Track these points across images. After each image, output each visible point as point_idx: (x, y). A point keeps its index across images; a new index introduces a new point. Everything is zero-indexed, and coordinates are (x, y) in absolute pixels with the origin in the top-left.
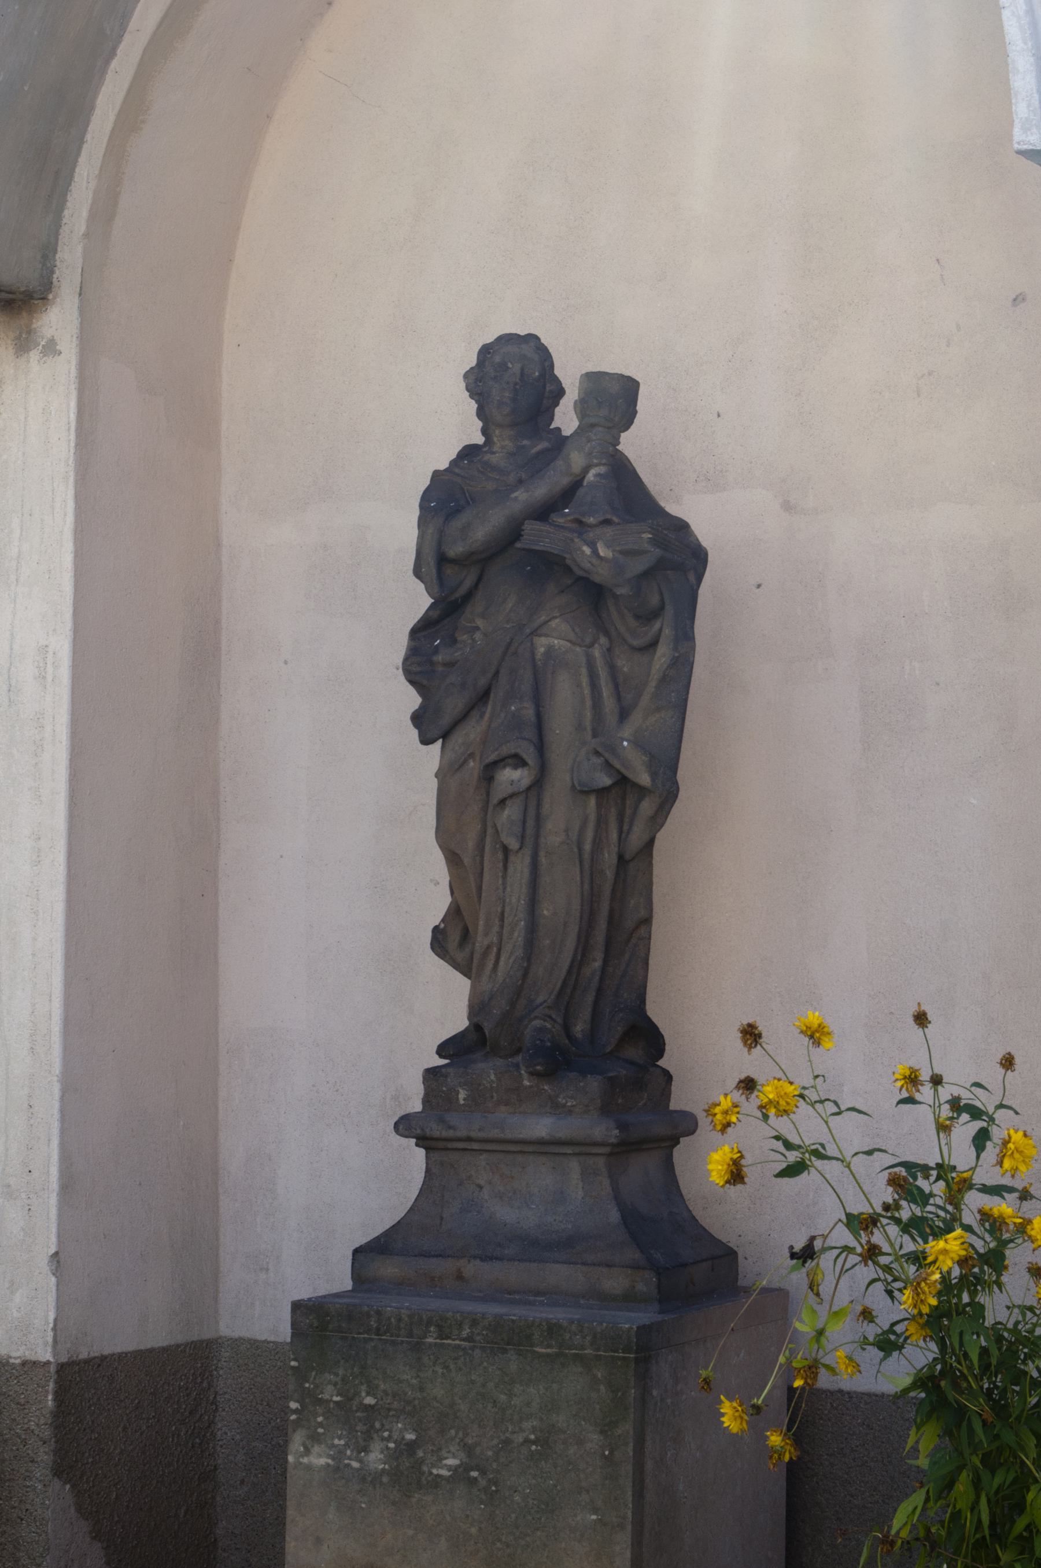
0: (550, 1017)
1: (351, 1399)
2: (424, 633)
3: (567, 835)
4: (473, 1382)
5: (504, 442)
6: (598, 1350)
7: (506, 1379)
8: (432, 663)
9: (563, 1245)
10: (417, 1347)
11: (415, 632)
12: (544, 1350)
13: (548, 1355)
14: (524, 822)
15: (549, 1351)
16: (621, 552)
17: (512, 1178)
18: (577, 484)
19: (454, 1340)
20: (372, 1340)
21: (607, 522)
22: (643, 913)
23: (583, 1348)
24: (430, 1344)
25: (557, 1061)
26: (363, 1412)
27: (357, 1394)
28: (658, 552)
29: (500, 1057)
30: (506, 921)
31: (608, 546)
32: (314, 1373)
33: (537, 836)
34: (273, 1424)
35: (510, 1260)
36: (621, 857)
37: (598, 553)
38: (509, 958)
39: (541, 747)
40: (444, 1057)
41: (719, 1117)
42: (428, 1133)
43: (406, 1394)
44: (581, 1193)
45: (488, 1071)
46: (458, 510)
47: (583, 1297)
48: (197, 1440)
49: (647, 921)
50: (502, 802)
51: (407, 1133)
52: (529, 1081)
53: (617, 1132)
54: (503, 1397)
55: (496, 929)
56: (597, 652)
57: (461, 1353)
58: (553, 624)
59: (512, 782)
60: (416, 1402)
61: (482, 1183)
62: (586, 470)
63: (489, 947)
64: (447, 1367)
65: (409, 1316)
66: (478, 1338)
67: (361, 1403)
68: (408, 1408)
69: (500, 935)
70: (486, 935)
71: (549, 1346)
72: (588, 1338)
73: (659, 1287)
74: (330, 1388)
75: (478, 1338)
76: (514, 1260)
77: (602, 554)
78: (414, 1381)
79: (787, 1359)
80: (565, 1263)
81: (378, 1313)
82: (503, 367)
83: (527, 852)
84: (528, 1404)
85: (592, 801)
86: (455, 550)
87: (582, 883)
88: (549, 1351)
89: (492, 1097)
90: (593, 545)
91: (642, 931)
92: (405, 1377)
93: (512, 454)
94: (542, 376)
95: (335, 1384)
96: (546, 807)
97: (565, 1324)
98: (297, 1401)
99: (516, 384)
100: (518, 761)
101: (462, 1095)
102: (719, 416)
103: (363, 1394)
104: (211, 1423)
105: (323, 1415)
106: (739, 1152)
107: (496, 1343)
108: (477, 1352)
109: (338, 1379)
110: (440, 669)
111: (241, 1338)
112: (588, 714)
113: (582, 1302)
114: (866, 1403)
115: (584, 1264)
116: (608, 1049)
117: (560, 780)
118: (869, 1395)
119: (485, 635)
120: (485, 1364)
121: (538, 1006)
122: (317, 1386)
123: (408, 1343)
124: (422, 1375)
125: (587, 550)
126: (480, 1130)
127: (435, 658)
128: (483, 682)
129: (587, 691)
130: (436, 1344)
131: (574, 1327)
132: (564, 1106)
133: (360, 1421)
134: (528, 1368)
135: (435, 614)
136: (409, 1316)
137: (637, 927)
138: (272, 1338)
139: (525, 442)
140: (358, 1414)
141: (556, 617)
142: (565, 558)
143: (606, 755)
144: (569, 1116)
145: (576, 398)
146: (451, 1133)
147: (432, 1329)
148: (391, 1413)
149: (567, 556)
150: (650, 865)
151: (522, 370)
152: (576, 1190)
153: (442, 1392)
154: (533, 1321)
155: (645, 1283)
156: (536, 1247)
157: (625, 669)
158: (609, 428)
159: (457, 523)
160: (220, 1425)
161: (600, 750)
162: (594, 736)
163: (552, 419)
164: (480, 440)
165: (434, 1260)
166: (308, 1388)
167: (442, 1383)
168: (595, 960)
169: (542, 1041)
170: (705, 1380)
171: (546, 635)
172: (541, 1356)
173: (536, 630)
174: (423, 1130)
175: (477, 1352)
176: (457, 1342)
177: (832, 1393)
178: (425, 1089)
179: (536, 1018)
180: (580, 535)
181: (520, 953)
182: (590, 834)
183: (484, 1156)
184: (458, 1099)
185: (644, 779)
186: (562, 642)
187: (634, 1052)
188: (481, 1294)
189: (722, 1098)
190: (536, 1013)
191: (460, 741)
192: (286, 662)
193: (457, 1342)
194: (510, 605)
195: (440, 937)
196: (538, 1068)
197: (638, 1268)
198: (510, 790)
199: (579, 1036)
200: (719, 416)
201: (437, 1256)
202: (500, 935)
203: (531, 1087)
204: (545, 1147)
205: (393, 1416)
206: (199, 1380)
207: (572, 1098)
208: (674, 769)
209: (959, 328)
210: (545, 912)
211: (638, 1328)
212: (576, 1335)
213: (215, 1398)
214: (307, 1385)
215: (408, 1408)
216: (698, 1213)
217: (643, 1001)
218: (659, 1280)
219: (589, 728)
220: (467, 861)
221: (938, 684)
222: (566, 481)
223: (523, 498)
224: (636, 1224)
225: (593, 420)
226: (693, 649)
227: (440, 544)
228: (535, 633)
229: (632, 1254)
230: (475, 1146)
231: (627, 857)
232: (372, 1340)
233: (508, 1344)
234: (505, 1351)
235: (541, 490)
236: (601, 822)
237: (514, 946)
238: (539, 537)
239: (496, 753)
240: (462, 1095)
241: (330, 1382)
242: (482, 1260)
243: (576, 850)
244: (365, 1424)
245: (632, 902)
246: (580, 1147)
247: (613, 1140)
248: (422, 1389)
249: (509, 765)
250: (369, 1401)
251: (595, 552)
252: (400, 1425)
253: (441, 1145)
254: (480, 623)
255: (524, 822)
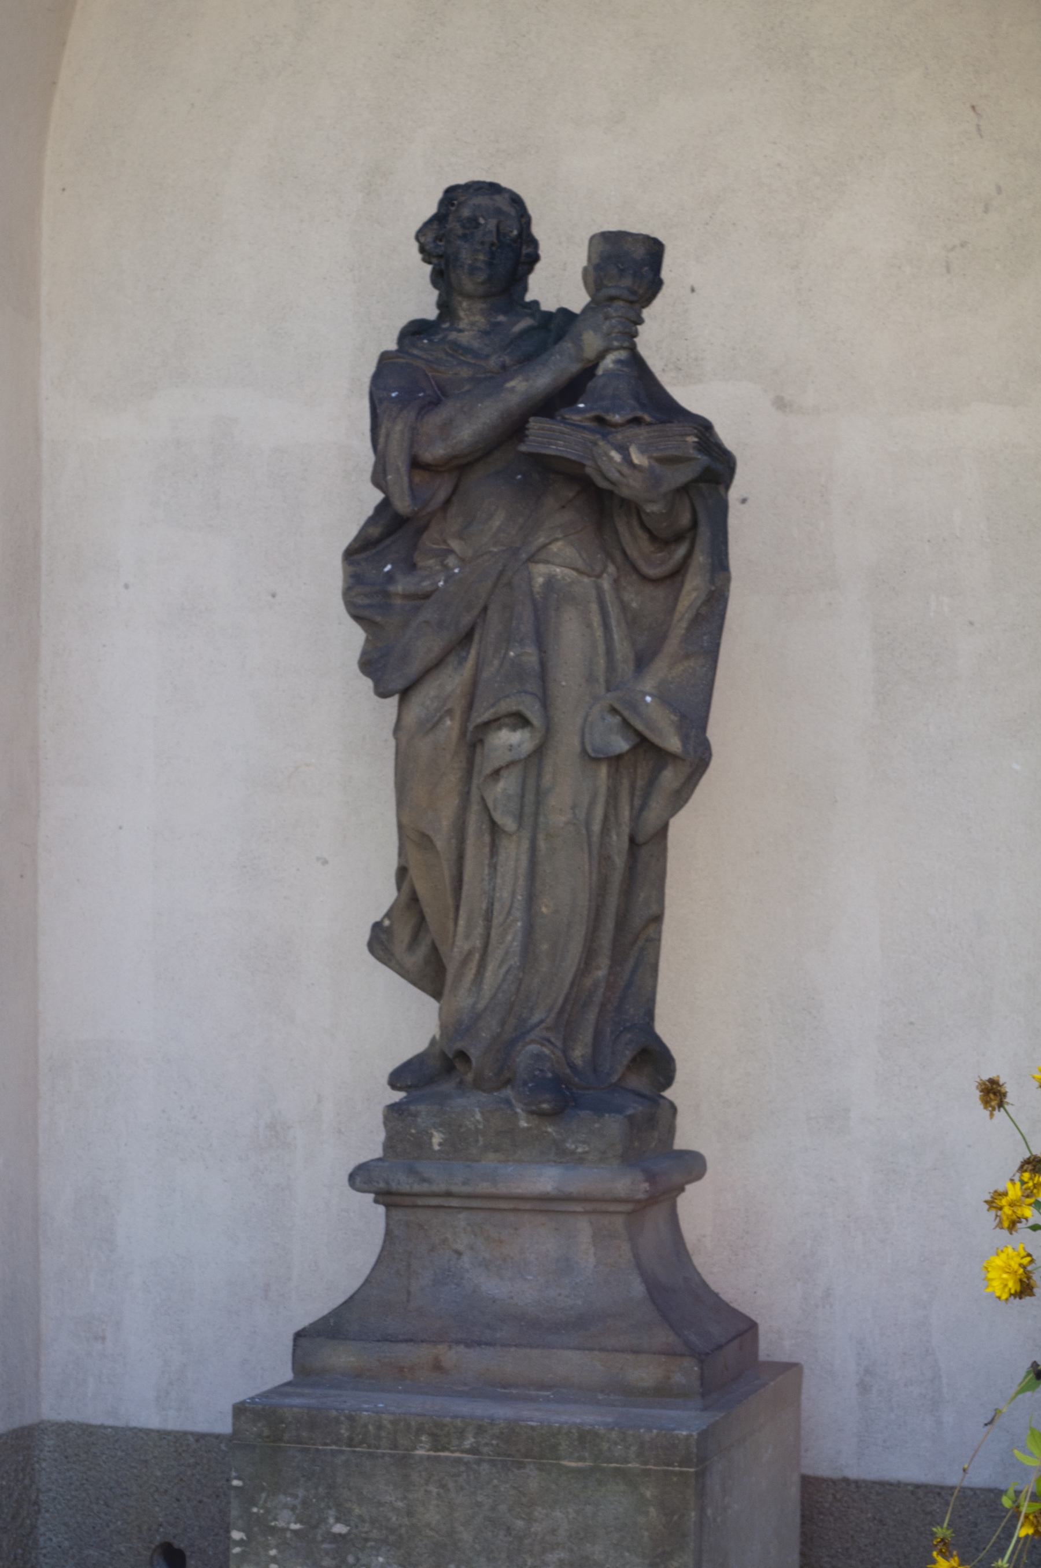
0: (549, 1041)
1: (316, 1527)
2: (363, 555)
3: (574, 813)
4: (479, 1505)
5: (471, 318)
6: (646, 1463)
7: (524, 1500)
8: (387, 594)
9: (578, 1326)
10: (404, 1461)
11: (350, 554)
12: (573, 1464)
13: (579, 1470)
14: (523, 796)
15: (580, 1464)
16: (660, 460)
17: (501, 1242)
18: (589, 371)
19: (452, 1452)
20: (342, 1452)
21: (637, 421)
22: (654, 909)
23: (626, 1461)
24: (421, 1457)
25: (563, 1096)
26: (330, 1543)
27: (323, 1520)
28: (704, 459)
29: (484, 1091)
30: (495, 922)
31: (642, 451)
32: (264, 1495)
33: (536, 814)
34: (112, 1527)
35: (503, 1345)
36: (632, 840)
37: (627, 461)
38: (500, 967)
39: (545, 702)
40: (400, 1089)
41: (1007, 1210)
42: (394, 1187)
43: (389, 1520)
44: (592, 1260)
45: (473, 1110)
46: (434, 403)
47: (602, 1392)
48: (20, 1551)
49: (657, 919)
50: (496, 773)
51: (366, 1187)
52: (528, 1122)
53: (646, 1186)
54: (520, 1523)
55: (479, 930)
56: (606, 584)
57: (463, 1468)
58: (554, 547)
59: (511, 748)
60: (403, 1530)
61: (461, 1247)
62: (601, 356)
63: (470, 953)
64: (443, 1486)
65: (392, 1422)
66: (485, 1450)
67: (329, 1533)
68: (392, 1538)
69: (487, 937)
70: (467, 936)
71: (581, 1459)
72: (634, 1449)
73: (702, 1378)
74: (286, 1514)
75: (485, 1450)
76: (510, 1346)
77: (636, 461)
78: (400, 1504)
79: (1014, 1502)
80: (579, 1349)
81: (351, 1418)
82: (473, 222)
83: (526, 834)
84: (553, 1531)
85: (603, 770)
86: (435, 452)
87: (591, 873)
88: (580, 1464)
89: (477, 1141)
90: (623, 450)
91: (651, 931)
92: (388, 1498)
93: (485, 333)
94: (520, 235)
95: (293, 1509)
96: (547, 780)
97: (602, 1430)
98: (240, 1530)
99: (493, 244)
100: (520, 720)
101: (437, 1139)
102: (693, 290)
103: (331, 1520)
104: (34, 1527)
105: (277, 1547)
106: (1029, 1255)
107: (509, 1456)
108: (485, 1466)
109: (297, 1502)
110: (398, 602)
111: (69, 1423)
112: (602, 662)
113: (600, 1397)
114: (878, 1494)
115: (602, 1350)
116: (615, 1079)
117: (567, 744)
118: (882, 1484)
119: (462, 560)
120: (495, 1482)
121: (533, 1028)
122: (268, 1511)
123: (392, 1456)
124: (410, 1496)
125: (616, 456)
126: (464, 1184)
127: (392, 588)
128: (466, 620)
129: (599, 633)
130: (429, 1457)
131: (614, 1435)
132: (573, 1153)
133: (327, 1554)
134: (554, 1487)
135: (375, 532)
136: (392, 1422)
137: (645, 927)
138: (110, 1422)
139: (501, 318)
140: (325, 1546)
141: (557, 540)
142: (583, 466)
143: (626, 714)
144: (576, 1167)
145: (585, 263)
146: (425, 1188)
147: (423, 1438)
148: (370, 1544)
149: (588, 463)
150: (664, 850)
151: (498, 227)
152: (586, 1255)
153: (438, 1517)
154: (560, 1428)
155: (684, 1373)
156: (537, 1329)
157: (634, 605)
158: (632, 302)
159: (435, 419)
160: (42, 1529)
161: (617, 706)
162: (608, 690)
163: (525, 289)
164: (431, 313)
165: (403, 1346)
166: (256, 1514)
167: (438, 1506)
168: (598, 968)
169: (542, 1071)
170: (942, 1540)
171: (547, 562)
172: (570, 1471)
173: (533, 555)
174: (387, 1183)
175: (485, 1466)
176: (457, 1455)
177: (834, 1482)
178: (387, 1132)
179: (533, 1041)
180: (604, 436)
181: (515, 961)
182: (599, 812)
183: (463, 1216)
184: (431, 1144)
185: (673, 743)
186: (567, 571)
187: (638, 1082)
188: (466, 1389)
189: (1009, 1185)
190: (532, 1036)
191: (432, 693)
192: (126, 586)
193: (457, 1455)
194: (496, 523)
195: (384, 937)
196: (545, 1106)
197: (675, 1354)
198: (508, 757)
199: (579, 1062)
200: (693, 290)
201: (406, 1341)
202: (487, 937)
203: (529, 1129)
204: (547, 1204)
205: (372, 1547)
206: (21, 1476)
207: (584, 1142)
208: (704, 728)
209: (999, 190)
210: (544, 910)
211: (699, 1434)
212: (616, 1444)
213: (37, 1497)
214: (255, 1510)
215: (392, 1538)
216: (710, 1280)
217: (650, 1014)
218: (702, 1369)
219: (602, 680)
220: (440, 844)
221: (971, 623)
222: (575, 368)
223: (521, 388)
224: (659, 1294)
225: (613, 292)
226: (728, 580)
227: (412, 443)
228: (532, 559)
229: (663, 1337)
230: (454, 1202)
231: (640, 839)
232: (342, 1452)
233: (526, 1457)
234: (521, 1465)
235: (541, 379)
236: (613, 796)
237: (507, 953)
238: (546, 437)
239: (492, 710)
240: (437, 1139)
241: (285, 1506)
242: (467, 1345)
243: (584, 831)
244: (334, 1558)
245: (642, 895)
246: (592, 1204)
247: (641, 1196)
248: (410, 1514)
249: (506, 725)
250: (339, 1529)
251: (627, 459)
252: (381, 1559)
253: (408, 1201)
254: (455, 545)
255: (523, 796)
